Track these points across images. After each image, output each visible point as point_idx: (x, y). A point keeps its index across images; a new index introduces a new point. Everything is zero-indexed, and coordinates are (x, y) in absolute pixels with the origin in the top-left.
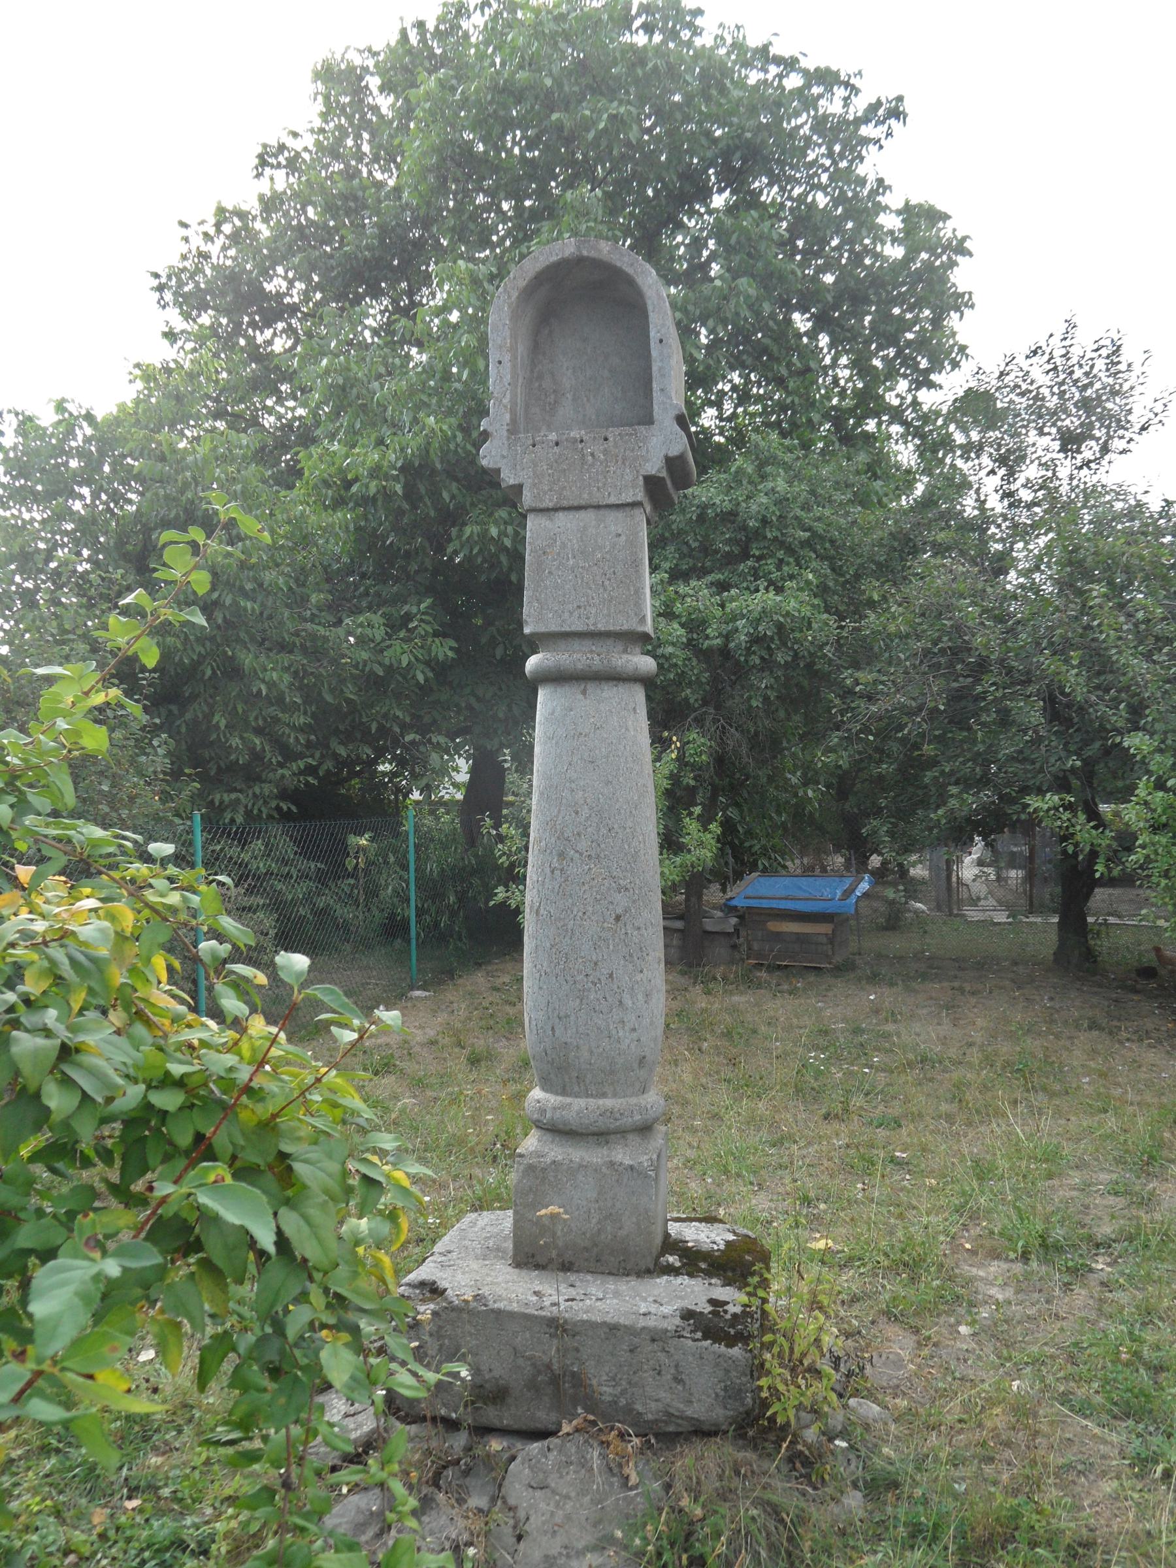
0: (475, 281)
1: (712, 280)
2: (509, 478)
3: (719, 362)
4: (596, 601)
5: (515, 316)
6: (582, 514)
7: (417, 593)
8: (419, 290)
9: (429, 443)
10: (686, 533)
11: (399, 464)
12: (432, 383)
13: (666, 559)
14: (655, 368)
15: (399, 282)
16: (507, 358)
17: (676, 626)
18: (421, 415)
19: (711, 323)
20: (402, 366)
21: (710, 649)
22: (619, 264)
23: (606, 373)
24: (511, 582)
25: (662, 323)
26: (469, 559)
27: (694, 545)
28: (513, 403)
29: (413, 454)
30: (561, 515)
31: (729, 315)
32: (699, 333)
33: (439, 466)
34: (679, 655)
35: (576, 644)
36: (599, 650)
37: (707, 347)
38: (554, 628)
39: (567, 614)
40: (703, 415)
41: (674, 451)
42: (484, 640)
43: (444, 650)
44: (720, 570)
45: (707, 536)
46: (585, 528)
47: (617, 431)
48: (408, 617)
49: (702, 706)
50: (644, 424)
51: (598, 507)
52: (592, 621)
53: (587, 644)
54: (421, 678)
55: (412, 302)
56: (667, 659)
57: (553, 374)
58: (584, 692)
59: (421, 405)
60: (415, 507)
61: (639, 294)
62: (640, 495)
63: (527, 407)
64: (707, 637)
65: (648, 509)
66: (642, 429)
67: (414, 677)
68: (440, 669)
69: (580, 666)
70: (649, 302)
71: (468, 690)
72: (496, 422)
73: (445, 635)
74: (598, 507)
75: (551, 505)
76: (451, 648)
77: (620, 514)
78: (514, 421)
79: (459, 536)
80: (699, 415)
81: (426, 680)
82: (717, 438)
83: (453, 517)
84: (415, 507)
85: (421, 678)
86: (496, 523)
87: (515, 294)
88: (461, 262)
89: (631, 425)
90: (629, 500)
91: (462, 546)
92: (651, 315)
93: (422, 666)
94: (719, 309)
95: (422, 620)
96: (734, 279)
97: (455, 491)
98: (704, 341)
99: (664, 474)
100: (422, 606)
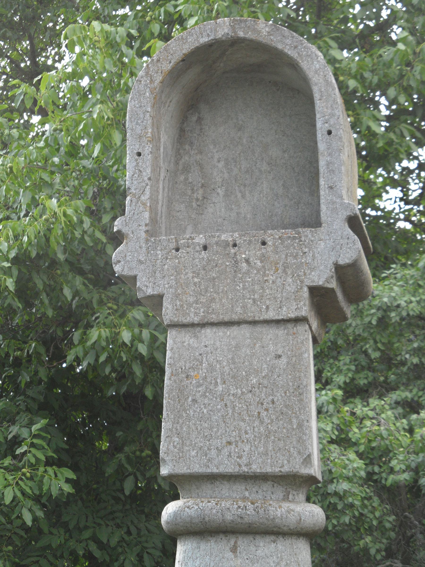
0: (112, 44)
1: (394, 44)
2: (146, 287)
3: (403, 136)
4: (250, 436)
5: (158, 102)
6: (234, 331)
7: (28, 410)
8: (44, 50)
9: (49, 230)
10: (364, 340)
11: (12, 255)
12: (56, 160)
13: (339, 371)
14: (322, 163)
15: (19, 40)
16: (147, 149)
17: (352, 456)
18: (42, 196)
19: (392, 92)
20: (20, 138)
21: (396, 486)
22: (280, 46)
23: (265, 167)
24: (145, 397)
25: (329, 108)
26: (94, 368)
27: (375, 355)
28: (154, 199)
29: (30, 243)
30: (208, 331)
31: (413, 84)
32: (377, 104)
33: (61, 257)
34: (356, 493)
35: (225, 489)
36: (254, 496)
37: (388, 118)
38: (197, 468)
39: (214, 452)
40: (385, 196)
41: (345, 259)
42: (109, 470)
43: (59, 482)
44: (406, 385)
45: (389, 345)
46: (238, 347)
47: (277, 233)
48: (17, 441)
49: (387, 557)
50: (310, 226)
51: (254, 323)
52: (244, 460)
53: (239, 489)
54: (28, 518)
55: (34, 63)
56: (341, 498)
57: (201, 167)
58: (234, 550)
59: (40, 185)
60: (28, 305)
61: (305, 79)
62: (304, 309)
63: (170, 202)
64: (392, 471)
65: (315, 324)
66: (307, 231)
67: (20, 517)
68: (54, 507)
69: (229, 517)
70: (315, 89)
71: (87, 534)
72: (132, 222)
73: (59, 463)
74: (254, 323)
75: (196, 320)
76: (68, 481)
77: (281, 332)
78: (154, 221)
79: (83, 341)
80: (380, 196)
81: (35, 519)
82: (402, 224)
83: (75, 317)
84: (28, 305)
85: (28, 518)
86: (130, 327)
87: (159, 78)
88: (95, 24)
89: (294, 226)
90: (292, 315)
91: (86, 354)
92: (318, 103)
93: (30, 503)
94: (402, 76)
95: (33, 445)
96: (419, 43)
97: (81, 287)
98: (385, 112)
99: (333, 284)
100: (34, 428)
